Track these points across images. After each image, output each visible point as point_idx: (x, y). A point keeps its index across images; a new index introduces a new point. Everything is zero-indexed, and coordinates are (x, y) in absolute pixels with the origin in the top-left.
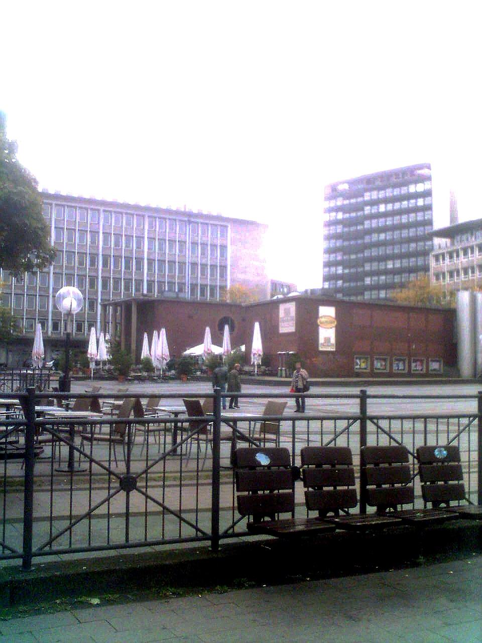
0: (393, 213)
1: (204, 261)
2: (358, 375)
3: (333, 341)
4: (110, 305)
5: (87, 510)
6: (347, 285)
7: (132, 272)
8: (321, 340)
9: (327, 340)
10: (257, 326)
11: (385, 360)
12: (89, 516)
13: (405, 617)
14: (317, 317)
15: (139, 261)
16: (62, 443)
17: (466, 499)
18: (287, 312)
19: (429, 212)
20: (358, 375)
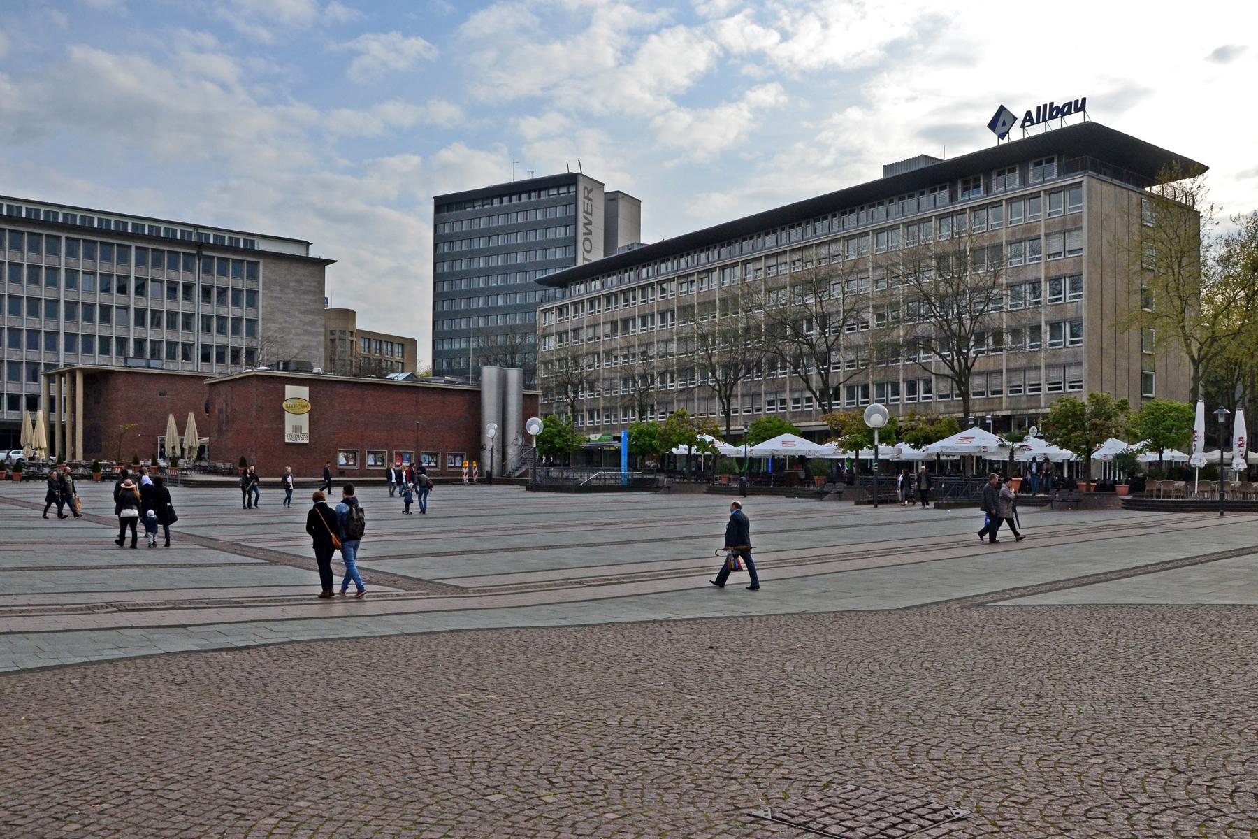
3: (306, 430)
8: (288, 429)
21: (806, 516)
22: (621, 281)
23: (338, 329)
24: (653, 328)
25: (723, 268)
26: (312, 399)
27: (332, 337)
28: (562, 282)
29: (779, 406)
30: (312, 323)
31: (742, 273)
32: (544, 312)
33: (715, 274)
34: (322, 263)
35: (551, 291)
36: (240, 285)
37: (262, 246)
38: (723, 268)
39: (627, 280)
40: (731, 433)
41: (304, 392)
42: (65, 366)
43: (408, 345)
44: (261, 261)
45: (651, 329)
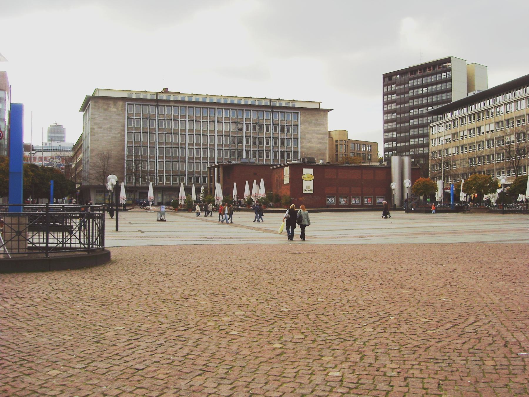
0: (431, 94)
1: (282, 136)
2: (328, 206)
3: (312, 188)
4: (214, 167)
5: (10, 239)
6: (399, 145)
7: (243, 145)
8: (304, 187)
9: (308, 187)
10: (235, 184)
11: (346, 198)
12: (11, 240)
13: (513, 374)
14: (302, 174)
15: (241, 138)
16: (6, 225)
17: (33, 234)
18: (286, 171)
19: (450, 93)
20: (328, 206)
21: (348, 235)
22: (493, 102)
23: (339, 140)
24: (513, 126)
25: (516, 101)
26: (315, 173)
27: (336, 144)
28: (442, 112)
29: (512, 174)
30: (323, 139)
31: (526, 103)
32: (432, 127)
33: (503, 107)
34: (327, 111)
35: (435, 117)
36: (290, 123)
37: (298, 105)
38: (516, 101)
39: (488, 104)
40: (50, 245)
41: (310, 171)
42: (217, 163)
43: (374, 145)
44: (299, 112)
45: (512, 126)
